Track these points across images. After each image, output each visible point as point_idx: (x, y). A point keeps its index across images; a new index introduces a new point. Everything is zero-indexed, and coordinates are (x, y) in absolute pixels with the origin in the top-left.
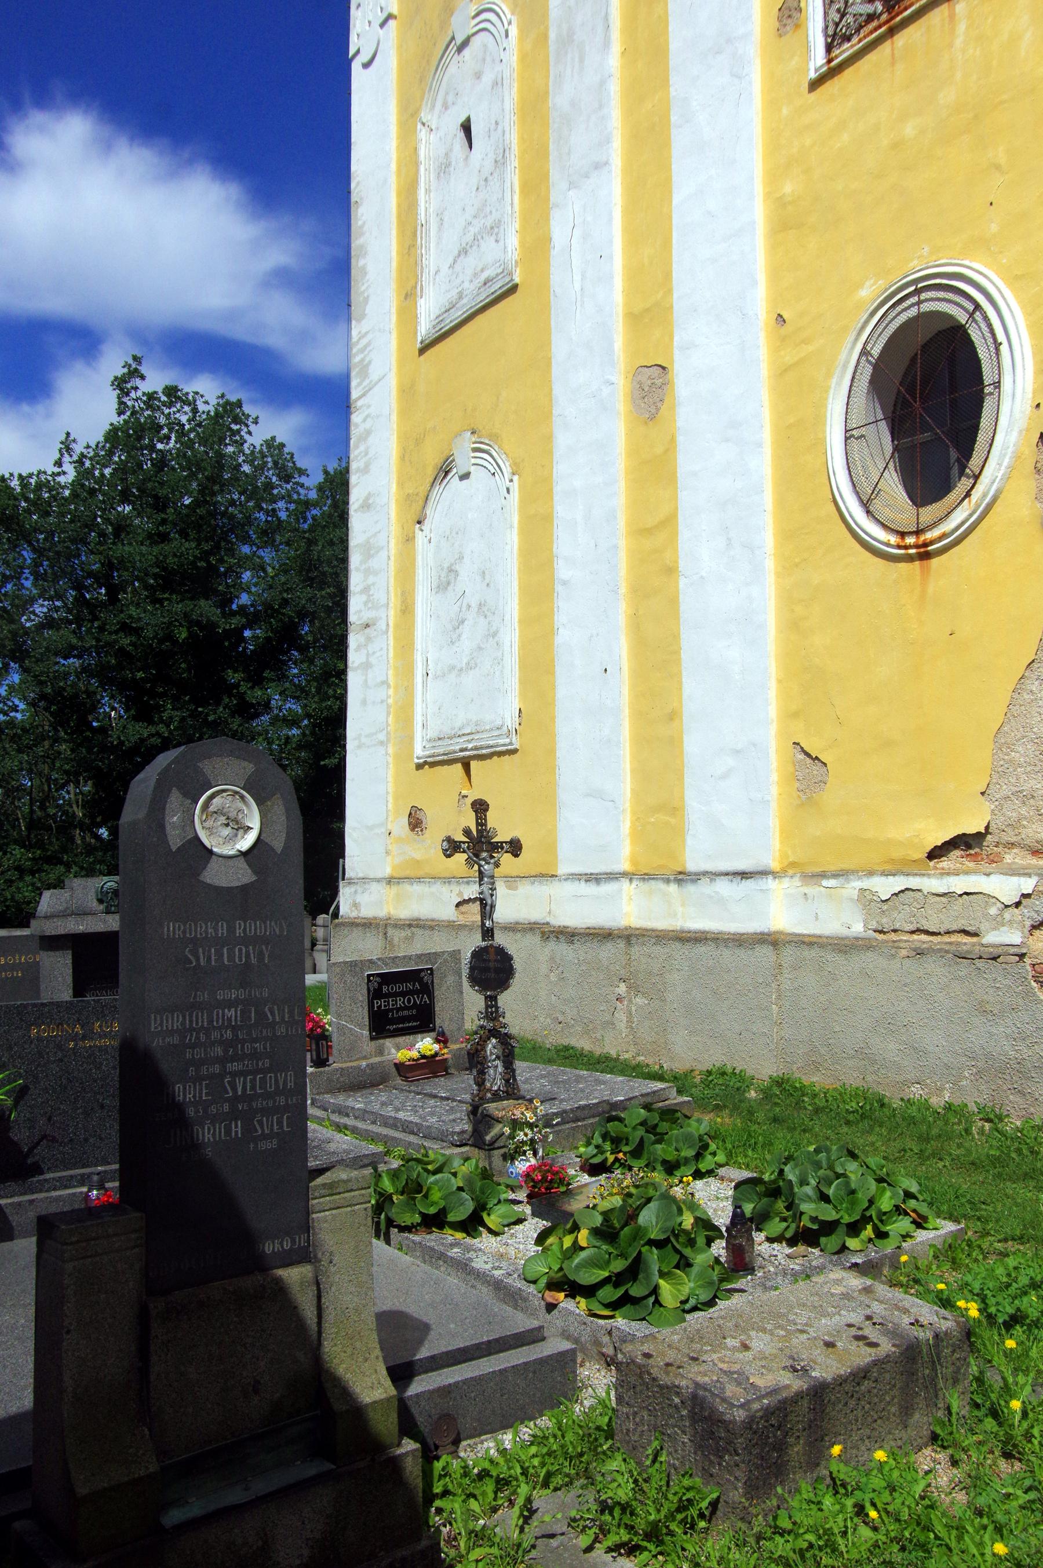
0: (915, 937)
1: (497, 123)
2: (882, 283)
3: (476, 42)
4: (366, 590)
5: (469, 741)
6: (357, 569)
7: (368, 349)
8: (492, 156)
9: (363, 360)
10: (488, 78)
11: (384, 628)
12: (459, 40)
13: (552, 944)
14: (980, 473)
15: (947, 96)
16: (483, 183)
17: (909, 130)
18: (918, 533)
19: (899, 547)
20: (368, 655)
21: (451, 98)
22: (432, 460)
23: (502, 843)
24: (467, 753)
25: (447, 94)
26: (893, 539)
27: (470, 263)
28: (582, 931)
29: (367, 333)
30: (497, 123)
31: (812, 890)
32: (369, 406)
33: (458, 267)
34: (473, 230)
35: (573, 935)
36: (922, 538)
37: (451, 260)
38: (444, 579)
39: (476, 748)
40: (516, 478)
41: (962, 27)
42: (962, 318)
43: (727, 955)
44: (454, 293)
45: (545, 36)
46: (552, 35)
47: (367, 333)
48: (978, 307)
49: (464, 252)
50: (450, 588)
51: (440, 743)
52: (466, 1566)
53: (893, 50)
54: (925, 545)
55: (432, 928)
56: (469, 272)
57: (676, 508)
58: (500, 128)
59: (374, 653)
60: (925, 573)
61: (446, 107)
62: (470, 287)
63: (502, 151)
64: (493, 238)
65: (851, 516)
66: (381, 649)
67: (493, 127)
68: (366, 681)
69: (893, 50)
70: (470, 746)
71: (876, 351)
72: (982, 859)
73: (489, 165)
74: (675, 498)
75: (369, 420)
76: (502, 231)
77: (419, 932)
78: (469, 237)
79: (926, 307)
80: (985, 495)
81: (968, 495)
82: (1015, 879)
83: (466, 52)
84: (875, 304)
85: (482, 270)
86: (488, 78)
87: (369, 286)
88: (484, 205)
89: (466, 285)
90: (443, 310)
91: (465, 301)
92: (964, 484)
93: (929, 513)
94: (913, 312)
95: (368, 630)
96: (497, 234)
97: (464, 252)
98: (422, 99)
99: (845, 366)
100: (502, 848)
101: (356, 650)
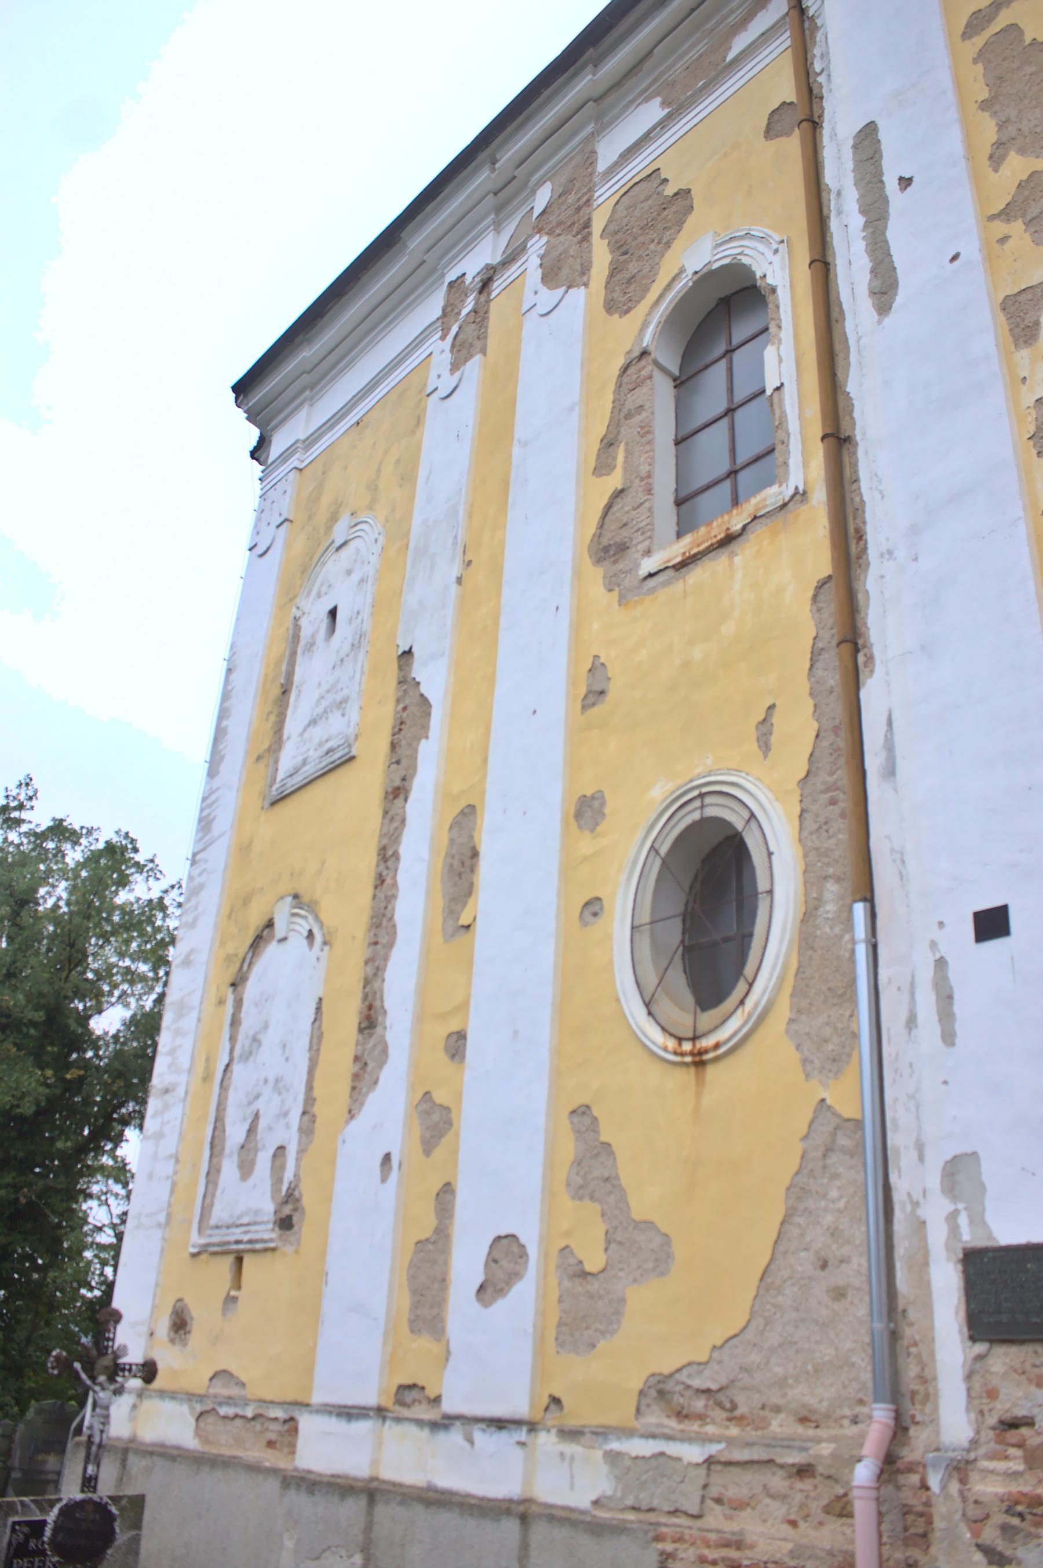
0: (674, 1520)
1: (358, 613)
2: (671, 786)
3: (353, 545)
4: (172, 1052)
5: (246, 1233)
6: (168, 1028)
7: (216, 805)
8: (350, 640)
9: (209, 815)
10: (356, 576)
11: (182, 1094)
12: (337, 544)
13: (292, 1495)
14: (754, 980)
15: (729, 629)
16: (339, 662)
17: (697, 653)
18: (694, 1039)
19: (675, 1053)
20: (163, 1124)
21: (324, 589)
22: (255, 920)
23: (131, 1365)
24: (241, 1247)
25: (322, 585)
26: (671, 1044)
27: (318, 733)
28: (325, 1479)
29: (218, 789)
30: (358, 613)
31: (571, 1448)
32: (206, 861)
33: (306, 735)
34: (324, 703)
35: (315, 1483)
36: (698, 1046)
37: (301, 729)
38: (247, 1048)
39: (250, 1242)
40: (326, 948)
41: (739, 575)
42: (739, 826)
43: (471, 1527)
44: (299, 759)
45: (407, 546)
46: (412, 545)
47: (218, 789)
48: (753, 815)
49: (313, 722)
50: (252, 1059)
51: (217, 1231)
52: (2, 828)
53: (685, 585)
54: (701, 1053)
55: (173, 1459)
56: (316, 740)
57: (469, 995)
58: (360, 618)
59: (169, 1122)
60: (700, 1081)
61: (319, 596)
62: (314, 755)
63: (358, 636)
64: (340, 713)
65: (634, 1019)
66: (176, 1119)
67: (355, 615)
68: (156, 1153)
69: (685, 585)
70: (246, 1238)
71: (664, 850)
72: (748, 1425)
73: (346, 647)
74: (469, 984)
75: (204, 874)
76: (348, 706)
77: (160, 1462)
78: (320, 710)
79: (711, 812)
80: (756, 1005)
81: (742, 1002)
82: (651, 1442)
83: (344, 553)
84: (669, 800)
85: (327, 741)
86: (356, 576)
87: (226, 746)
88: (337, 682)
89: (311, 753)
90: (288, 774)
91: (307, 768)
92: (741, 987)
93: (707, 1019)
94: (696, 816)
95: (167, 1097)
96: (344, 709)
97: (313, 722)
98: (301, 588)
99: (634, 863)
100: (130, 1370)
101: (154, 1116)
